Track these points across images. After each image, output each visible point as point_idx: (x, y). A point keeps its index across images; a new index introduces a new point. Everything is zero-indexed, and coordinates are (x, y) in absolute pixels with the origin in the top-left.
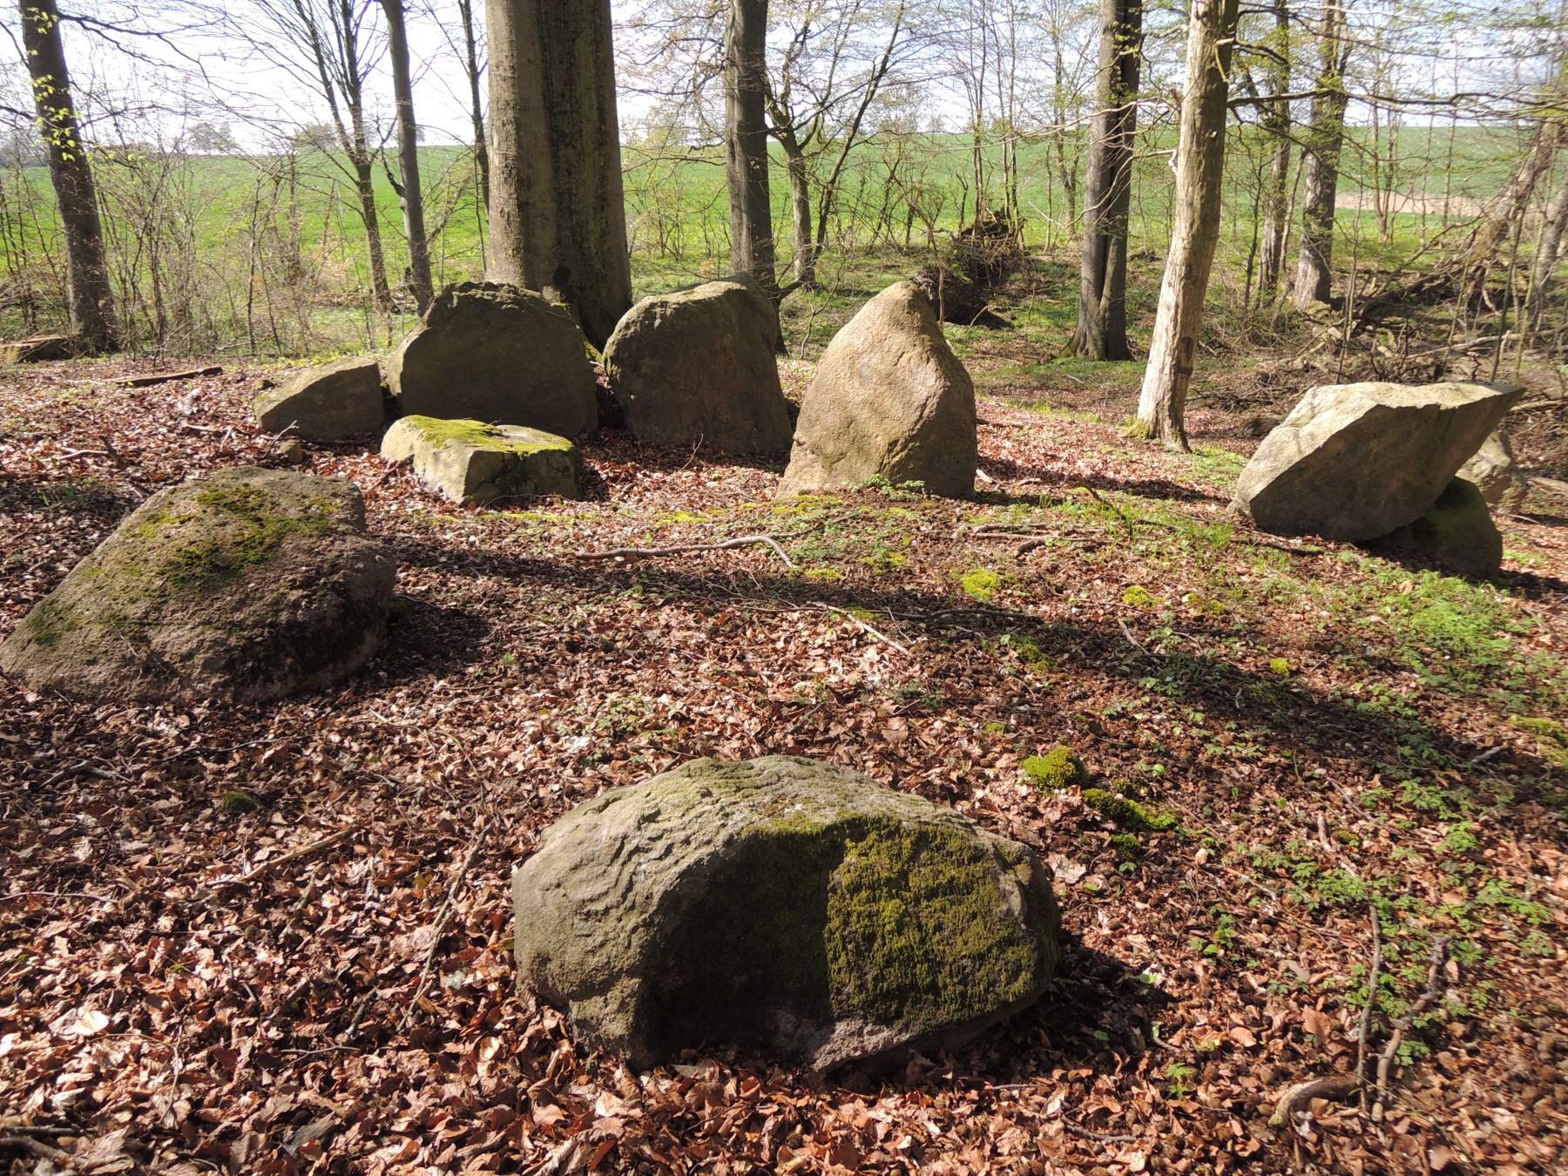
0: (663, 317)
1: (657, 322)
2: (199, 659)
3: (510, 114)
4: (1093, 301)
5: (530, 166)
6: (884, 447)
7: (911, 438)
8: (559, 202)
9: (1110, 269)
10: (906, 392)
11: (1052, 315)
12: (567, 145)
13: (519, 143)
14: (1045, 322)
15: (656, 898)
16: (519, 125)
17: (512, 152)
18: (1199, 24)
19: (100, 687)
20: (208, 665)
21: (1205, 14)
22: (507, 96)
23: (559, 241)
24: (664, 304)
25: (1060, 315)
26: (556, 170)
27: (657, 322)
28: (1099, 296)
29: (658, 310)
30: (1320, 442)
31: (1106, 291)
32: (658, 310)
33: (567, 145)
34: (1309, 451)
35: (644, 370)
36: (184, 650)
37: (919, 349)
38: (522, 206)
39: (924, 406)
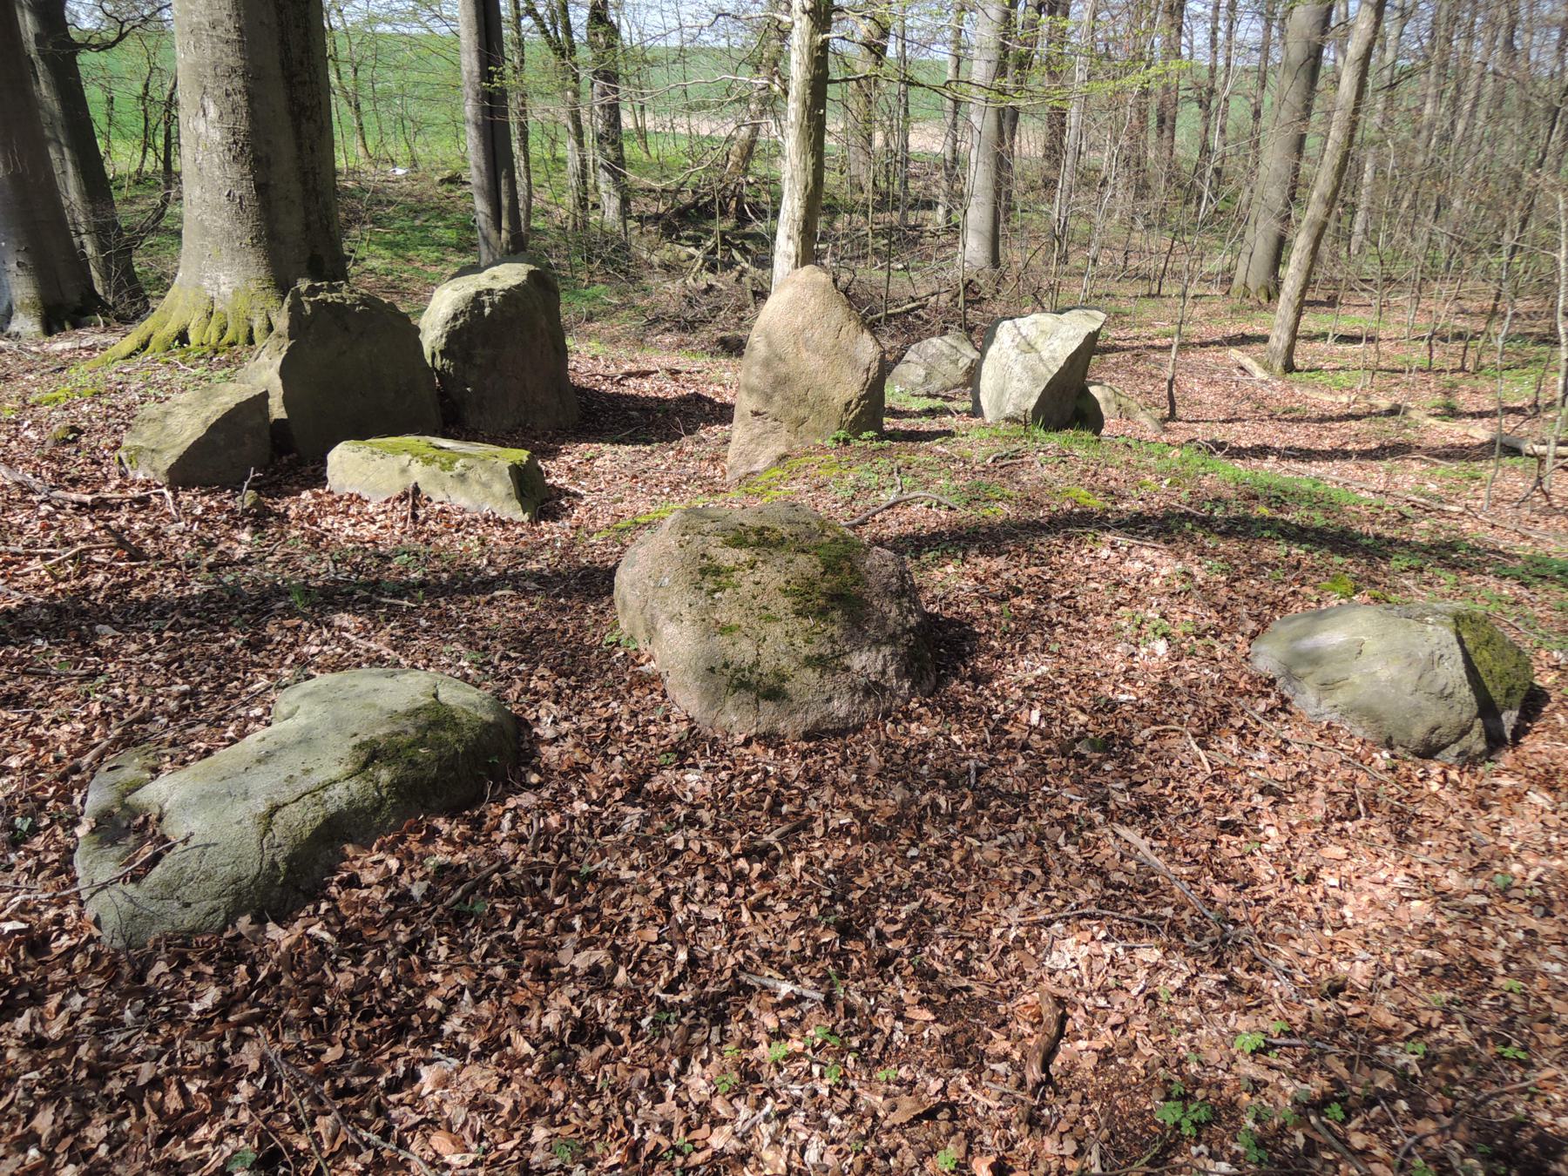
0: (492, 304)
1: (487, 311)
2: (891, 670)
3: (238, 83)
4: (493, 234)
5: (269, 142)
6: (840, 409)
7: (862, 398)
8: (305, 183)
9: (505, 202)
10: (853, 361)
11: (390, 245)
12: (308, 119)
13: (253, 115)
14: (387, 254)
15: (282, 867)
16: (251, 96)
17: (243, 126)
18: (806, 18)
19: (847, 717)
20: (899, 675)
21: (811, 10)
22: (233, 60)
23: (308, 226)
24: (490, 292)
25: (398, 245)
26: (300, 147)
27: (487, 311)
28: (499, 229)
29: (485, 298)
30: (1061, 363)
31: (505, 224)
32: (485, 298)
33: (308, 119)
34: (1056, 370)
35: (478, 361)
36: (879, 668)
37: (853, 323)
38: (262, 188)
39: (868, 370)
